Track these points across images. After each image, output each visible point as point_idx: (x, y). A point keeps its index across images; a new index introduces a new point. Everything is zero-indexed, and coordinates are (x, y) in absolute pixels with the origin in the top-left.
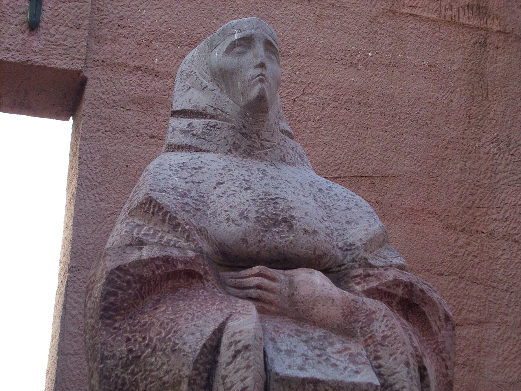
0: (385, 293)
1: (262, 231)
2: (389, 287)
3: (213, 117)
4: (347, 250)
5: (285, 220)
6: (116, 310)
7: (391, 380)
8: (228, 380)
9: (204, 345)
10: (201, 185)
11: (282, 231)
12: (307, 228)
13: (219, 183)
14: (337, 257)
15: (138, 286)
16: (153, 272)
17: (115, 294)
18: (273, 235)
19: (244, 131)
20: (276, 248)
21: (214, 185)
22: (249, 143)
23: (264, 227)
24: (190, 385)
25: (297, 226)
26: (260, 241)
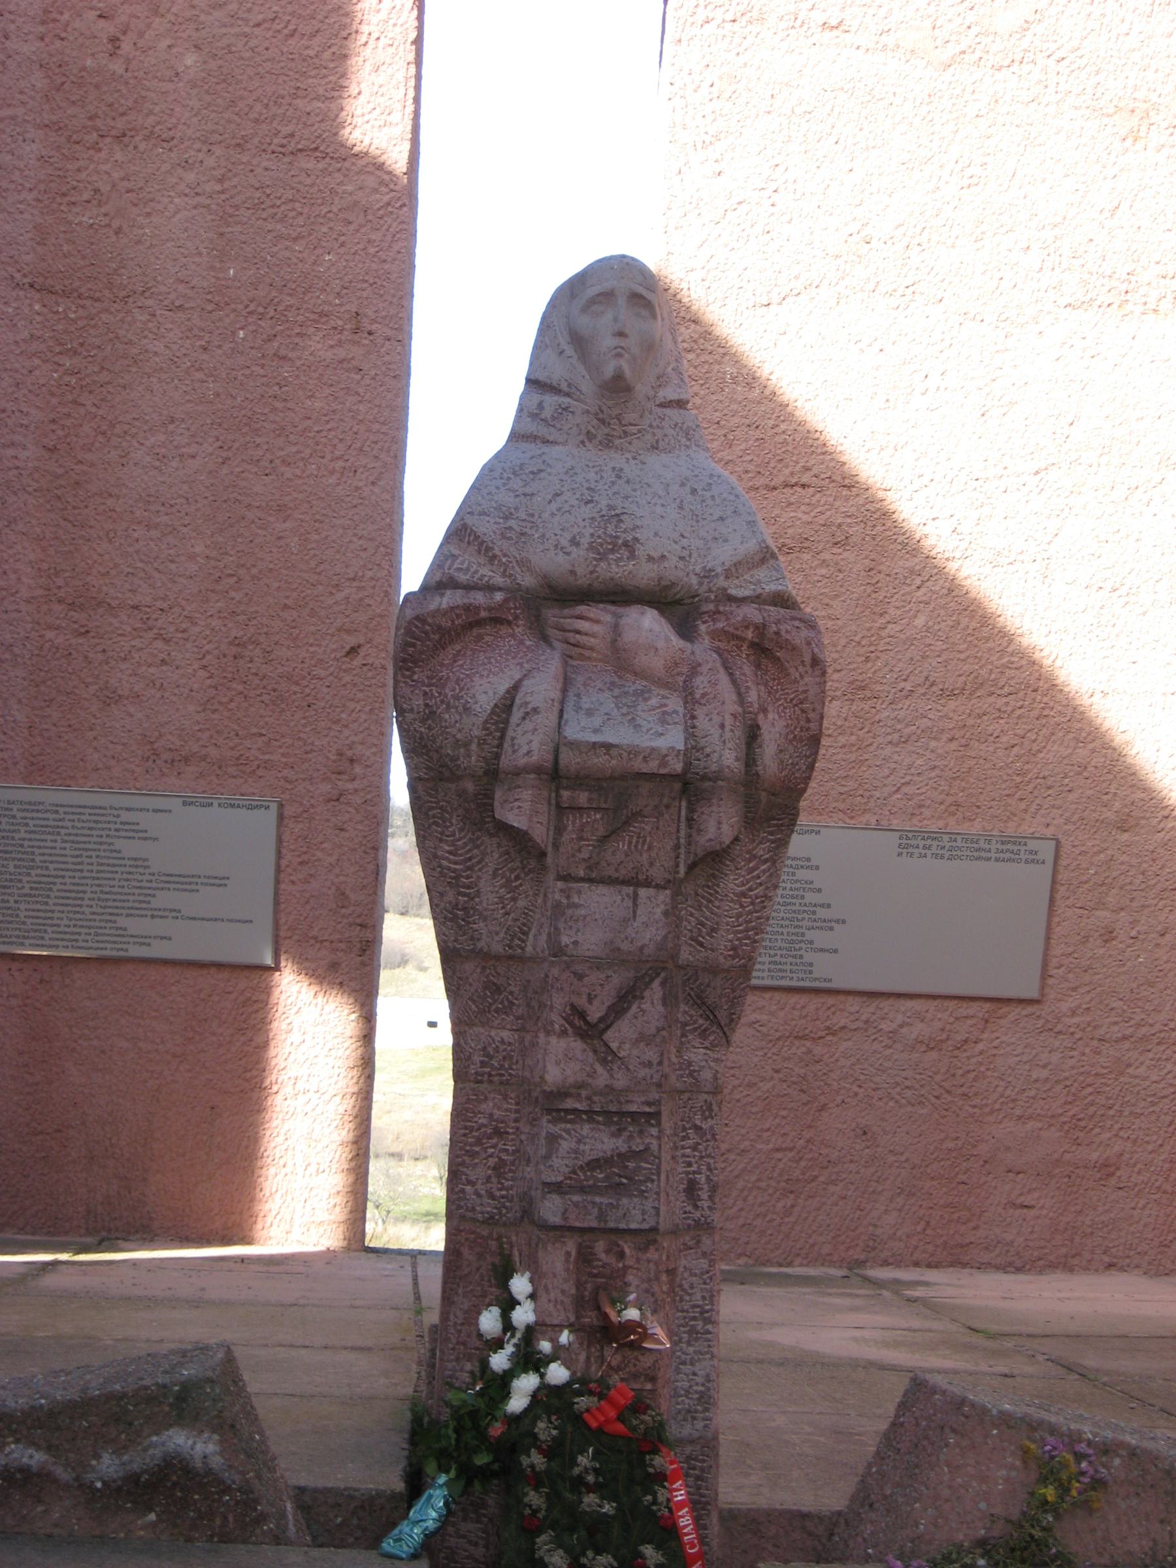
0: (733, 635)
1: (595, 559)
2: (737, 629)
3: (568, 395)
4: (705, 577)
5: (626, 544)
6: (414, 662)
7: (703, 742)
8: (516, 741)
9: (496, 705)
10: (534, 499)
11: (620, 559)
12: (652, 554)
13: (557, 495)
14: (690, 586)
15: (437, 637)
16: (453, 621)
17: (414, 645)
18: (609, 564)
19: (601, 416)
20: (612, 579)
21: (550, 497)
22: (606, 431)
23: (599, 554)
24: (479, 744)
25: (641, 551)
26: (592, 573)
